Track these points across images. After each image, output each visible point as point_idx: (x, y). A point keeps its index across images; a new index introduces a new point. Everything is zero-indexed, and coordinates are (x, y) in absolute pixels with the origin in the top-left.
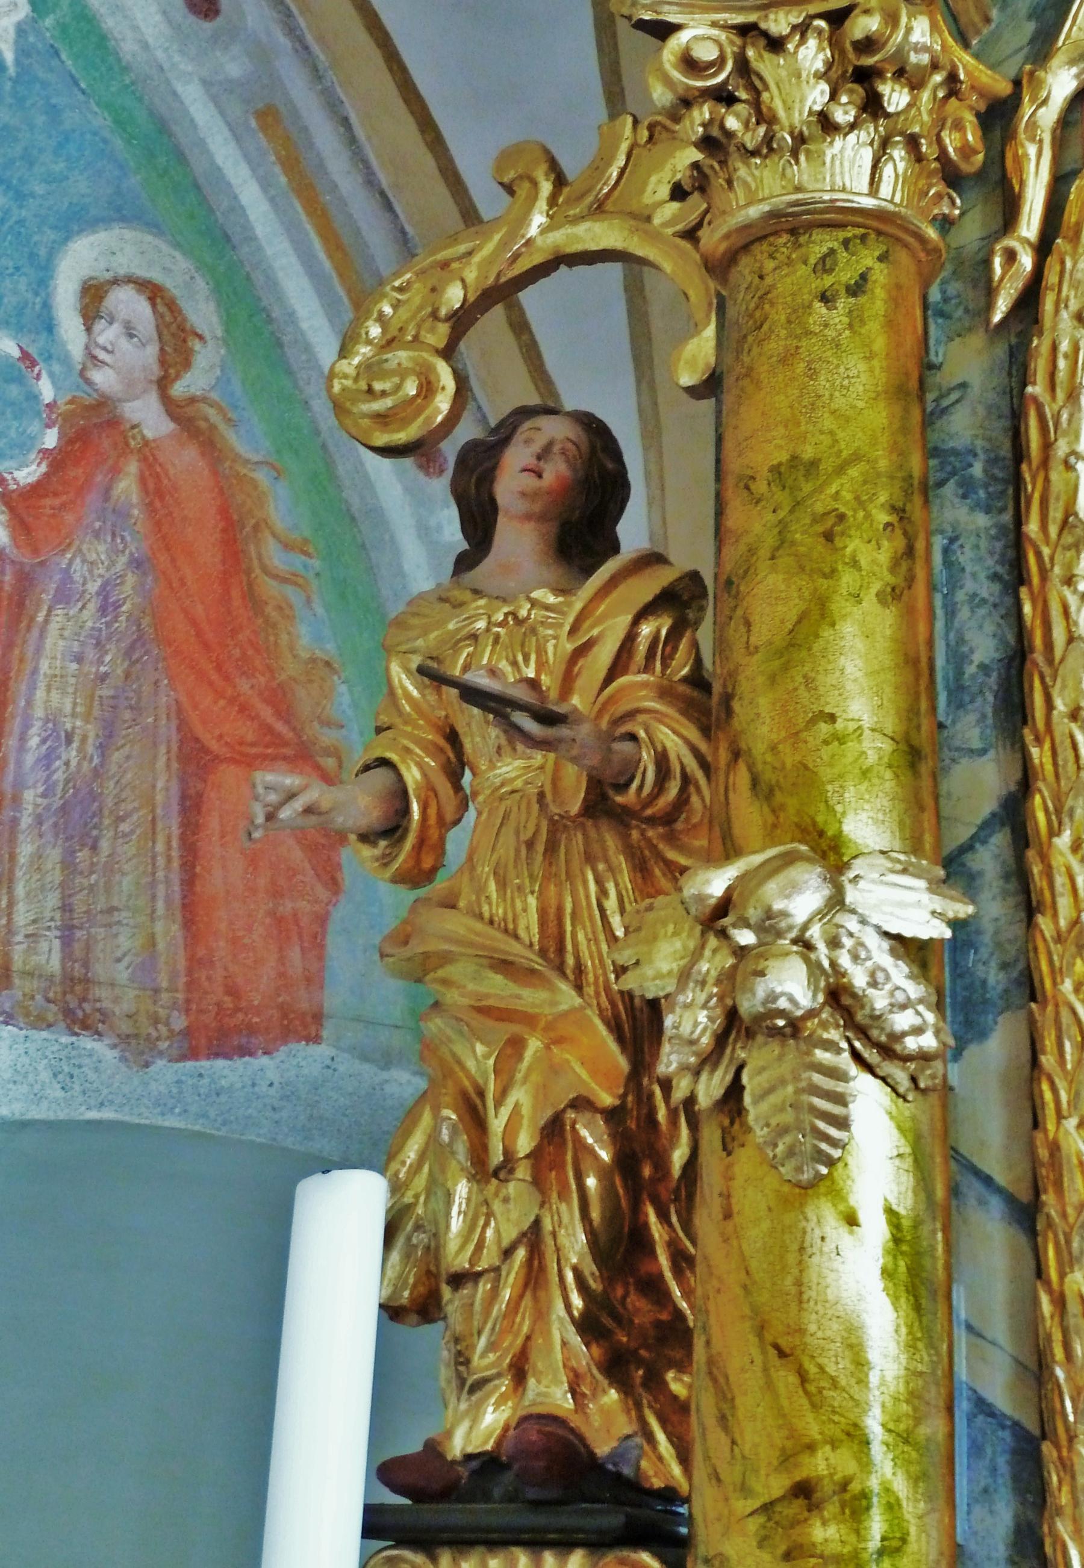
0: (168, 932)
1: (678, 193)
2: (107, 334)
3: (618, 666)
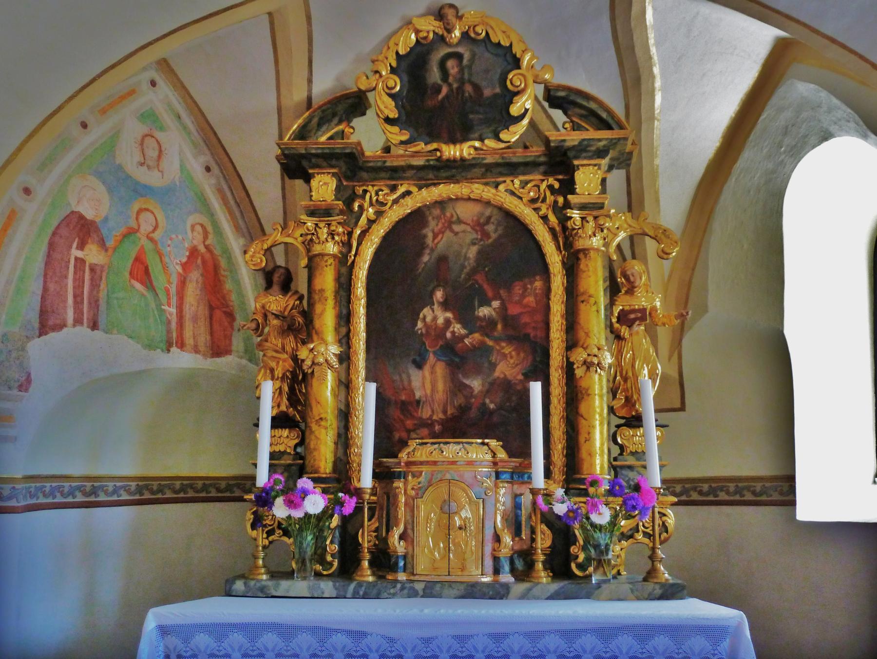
0: (208, 338)
1: (301, 235)
2: (195, 234)
3: (292, 309)
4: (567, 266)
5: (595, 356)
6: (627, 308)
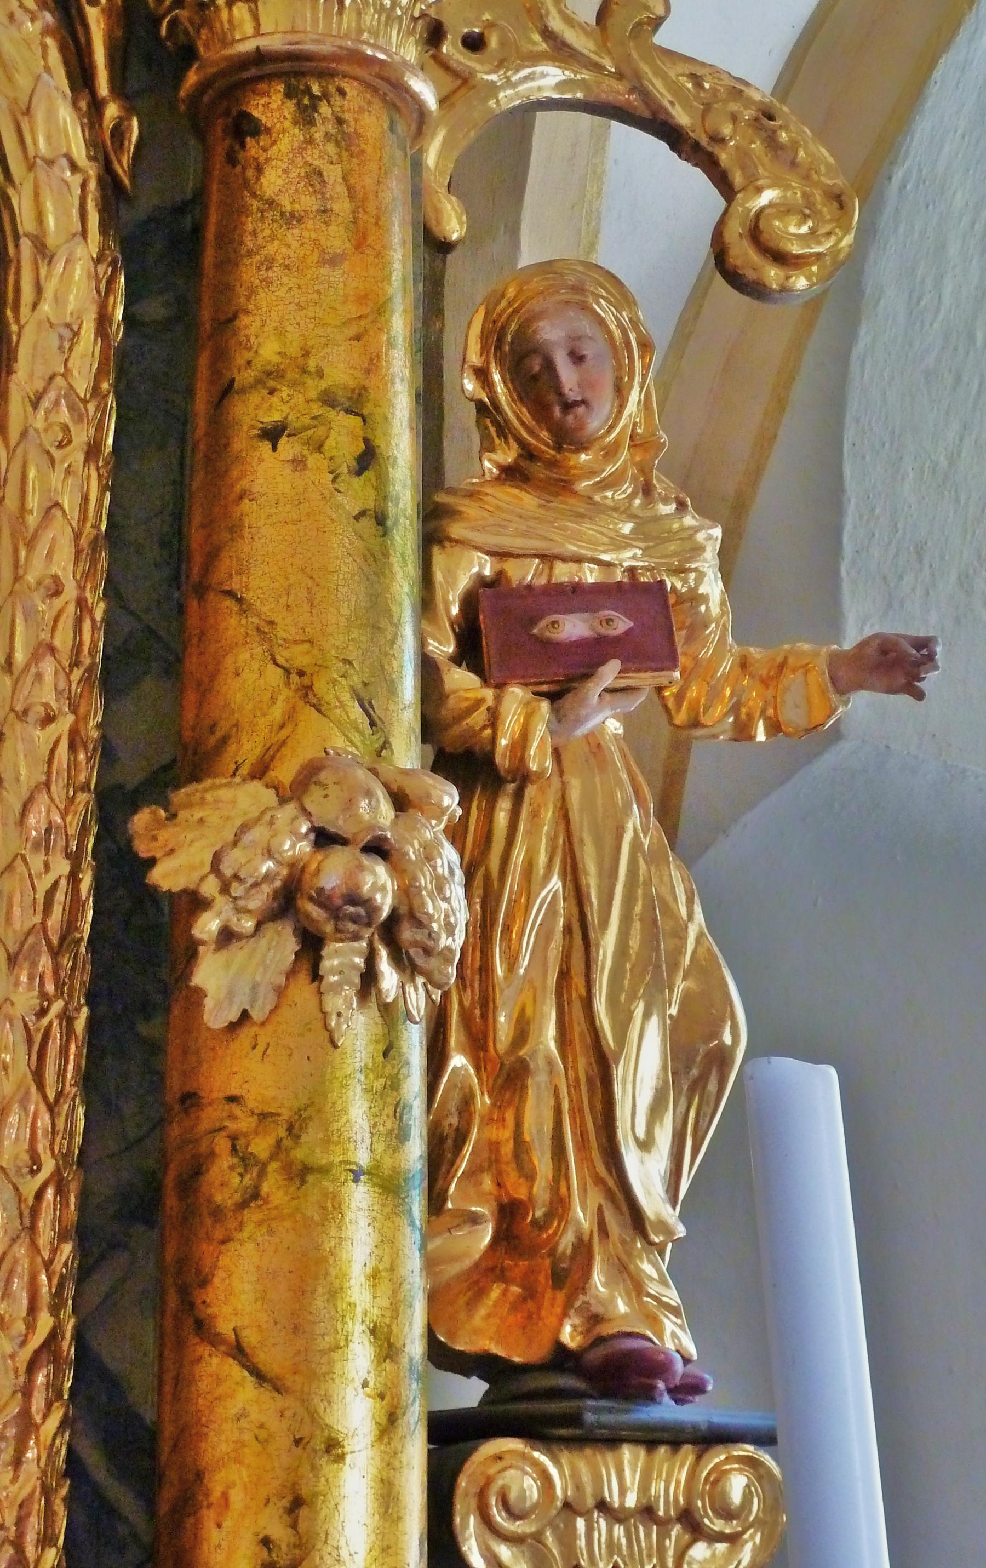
4: (130, 216)
5: (378, 849)
6: (526, 573)
